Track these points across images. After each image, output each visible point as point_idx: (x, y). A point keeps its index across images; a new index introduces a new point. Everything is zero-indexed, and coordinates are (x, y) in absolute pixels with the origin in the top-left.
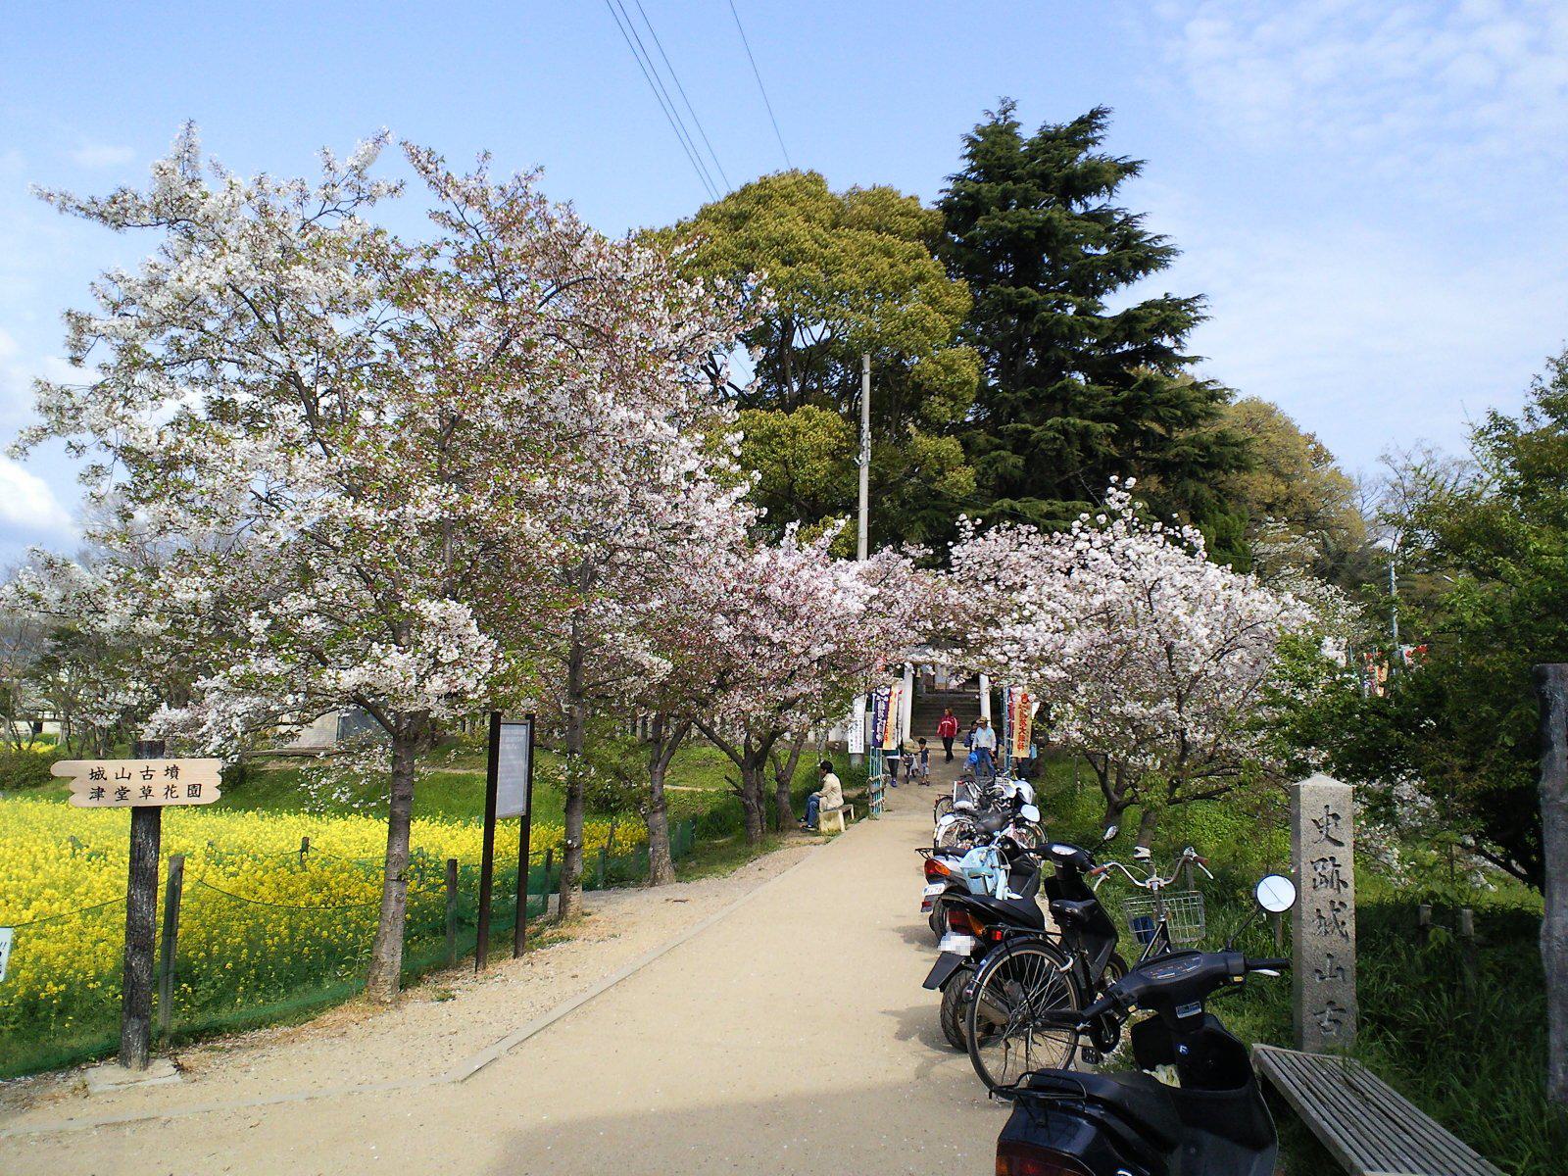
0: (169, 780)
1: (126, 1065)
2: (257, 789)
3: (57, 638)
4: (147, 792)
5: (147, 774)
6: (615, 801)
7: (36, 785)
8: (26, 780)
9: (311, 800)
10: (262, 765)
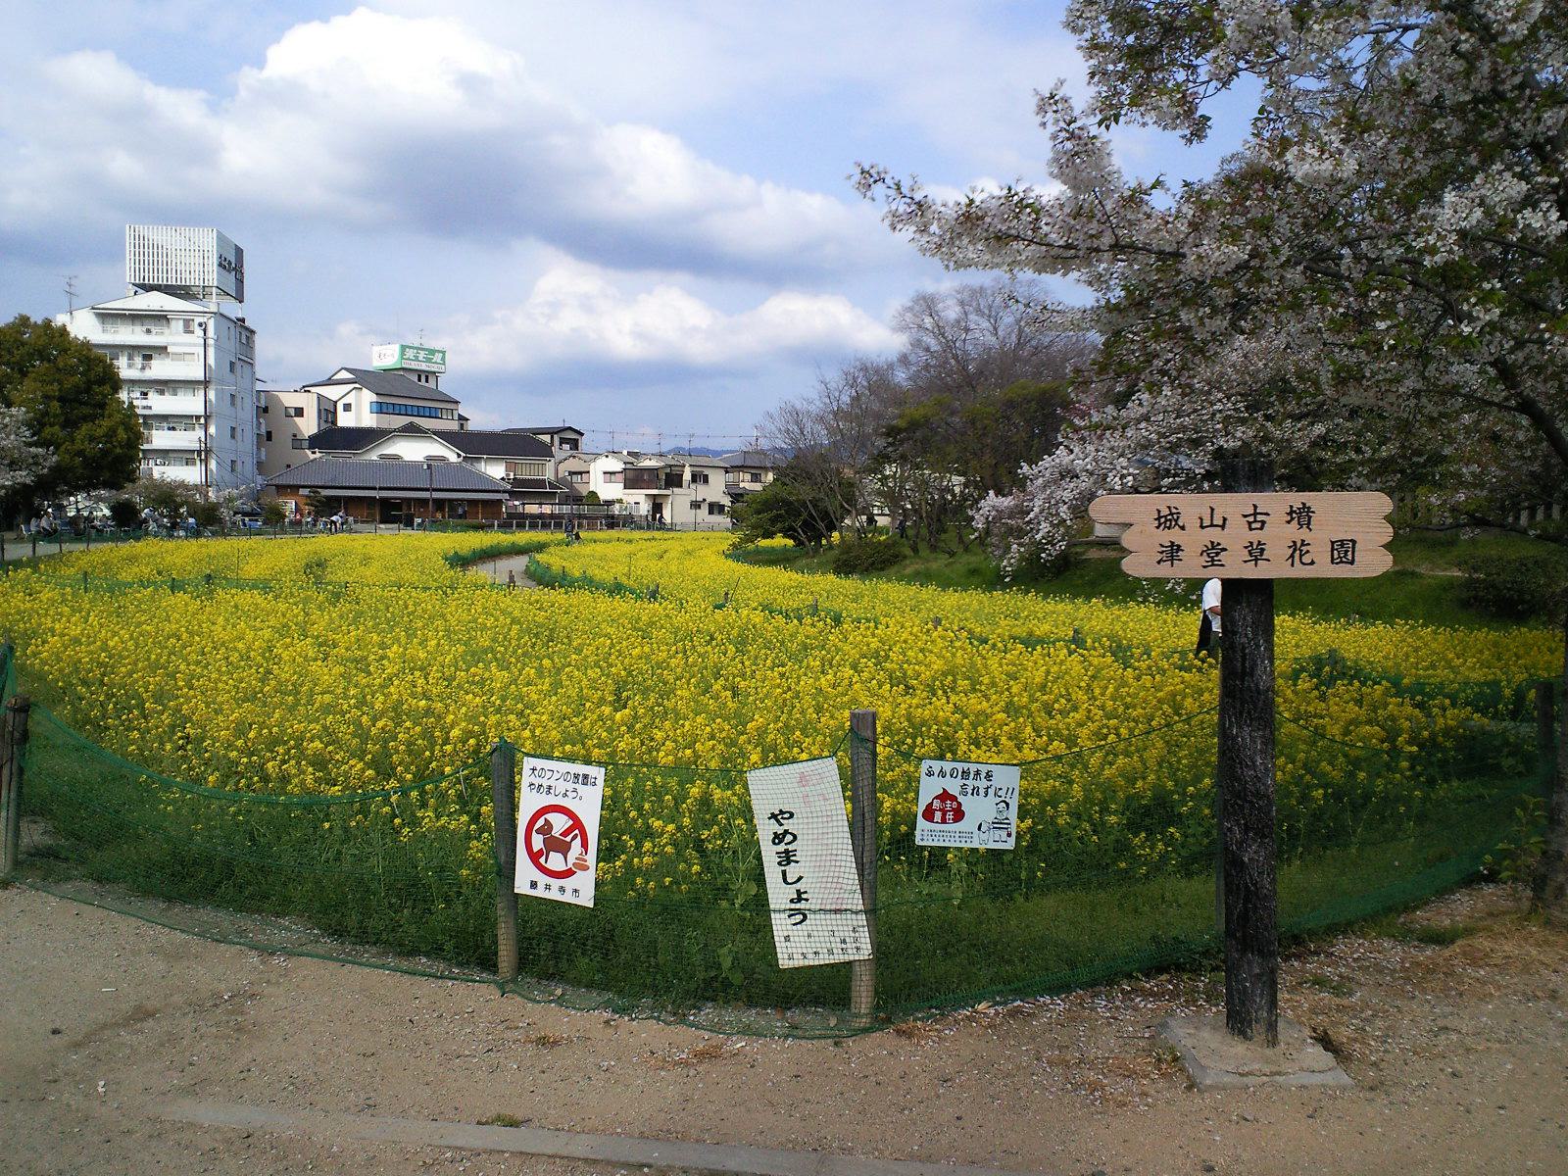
0: (1294, 532)
1: (1242, 1033)
2: (1082, 576)
3: (888, 435)
4: (1256, 552)
5: (1256, 519)
6: (1523, 602)
7: (882, 569)
8: (873, 563)
9: (1143, 589)
10: (1083, 553)
